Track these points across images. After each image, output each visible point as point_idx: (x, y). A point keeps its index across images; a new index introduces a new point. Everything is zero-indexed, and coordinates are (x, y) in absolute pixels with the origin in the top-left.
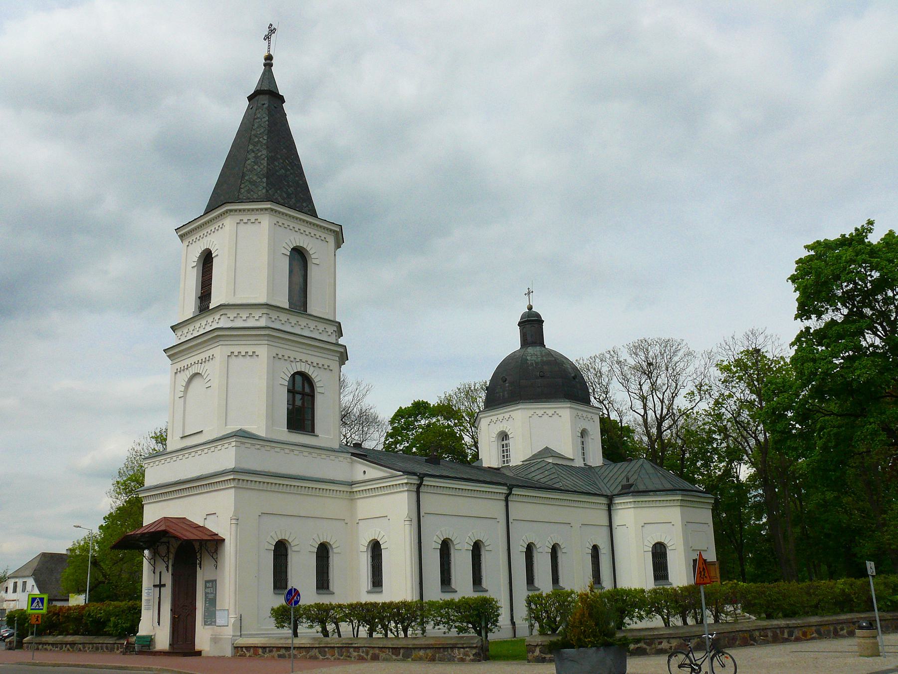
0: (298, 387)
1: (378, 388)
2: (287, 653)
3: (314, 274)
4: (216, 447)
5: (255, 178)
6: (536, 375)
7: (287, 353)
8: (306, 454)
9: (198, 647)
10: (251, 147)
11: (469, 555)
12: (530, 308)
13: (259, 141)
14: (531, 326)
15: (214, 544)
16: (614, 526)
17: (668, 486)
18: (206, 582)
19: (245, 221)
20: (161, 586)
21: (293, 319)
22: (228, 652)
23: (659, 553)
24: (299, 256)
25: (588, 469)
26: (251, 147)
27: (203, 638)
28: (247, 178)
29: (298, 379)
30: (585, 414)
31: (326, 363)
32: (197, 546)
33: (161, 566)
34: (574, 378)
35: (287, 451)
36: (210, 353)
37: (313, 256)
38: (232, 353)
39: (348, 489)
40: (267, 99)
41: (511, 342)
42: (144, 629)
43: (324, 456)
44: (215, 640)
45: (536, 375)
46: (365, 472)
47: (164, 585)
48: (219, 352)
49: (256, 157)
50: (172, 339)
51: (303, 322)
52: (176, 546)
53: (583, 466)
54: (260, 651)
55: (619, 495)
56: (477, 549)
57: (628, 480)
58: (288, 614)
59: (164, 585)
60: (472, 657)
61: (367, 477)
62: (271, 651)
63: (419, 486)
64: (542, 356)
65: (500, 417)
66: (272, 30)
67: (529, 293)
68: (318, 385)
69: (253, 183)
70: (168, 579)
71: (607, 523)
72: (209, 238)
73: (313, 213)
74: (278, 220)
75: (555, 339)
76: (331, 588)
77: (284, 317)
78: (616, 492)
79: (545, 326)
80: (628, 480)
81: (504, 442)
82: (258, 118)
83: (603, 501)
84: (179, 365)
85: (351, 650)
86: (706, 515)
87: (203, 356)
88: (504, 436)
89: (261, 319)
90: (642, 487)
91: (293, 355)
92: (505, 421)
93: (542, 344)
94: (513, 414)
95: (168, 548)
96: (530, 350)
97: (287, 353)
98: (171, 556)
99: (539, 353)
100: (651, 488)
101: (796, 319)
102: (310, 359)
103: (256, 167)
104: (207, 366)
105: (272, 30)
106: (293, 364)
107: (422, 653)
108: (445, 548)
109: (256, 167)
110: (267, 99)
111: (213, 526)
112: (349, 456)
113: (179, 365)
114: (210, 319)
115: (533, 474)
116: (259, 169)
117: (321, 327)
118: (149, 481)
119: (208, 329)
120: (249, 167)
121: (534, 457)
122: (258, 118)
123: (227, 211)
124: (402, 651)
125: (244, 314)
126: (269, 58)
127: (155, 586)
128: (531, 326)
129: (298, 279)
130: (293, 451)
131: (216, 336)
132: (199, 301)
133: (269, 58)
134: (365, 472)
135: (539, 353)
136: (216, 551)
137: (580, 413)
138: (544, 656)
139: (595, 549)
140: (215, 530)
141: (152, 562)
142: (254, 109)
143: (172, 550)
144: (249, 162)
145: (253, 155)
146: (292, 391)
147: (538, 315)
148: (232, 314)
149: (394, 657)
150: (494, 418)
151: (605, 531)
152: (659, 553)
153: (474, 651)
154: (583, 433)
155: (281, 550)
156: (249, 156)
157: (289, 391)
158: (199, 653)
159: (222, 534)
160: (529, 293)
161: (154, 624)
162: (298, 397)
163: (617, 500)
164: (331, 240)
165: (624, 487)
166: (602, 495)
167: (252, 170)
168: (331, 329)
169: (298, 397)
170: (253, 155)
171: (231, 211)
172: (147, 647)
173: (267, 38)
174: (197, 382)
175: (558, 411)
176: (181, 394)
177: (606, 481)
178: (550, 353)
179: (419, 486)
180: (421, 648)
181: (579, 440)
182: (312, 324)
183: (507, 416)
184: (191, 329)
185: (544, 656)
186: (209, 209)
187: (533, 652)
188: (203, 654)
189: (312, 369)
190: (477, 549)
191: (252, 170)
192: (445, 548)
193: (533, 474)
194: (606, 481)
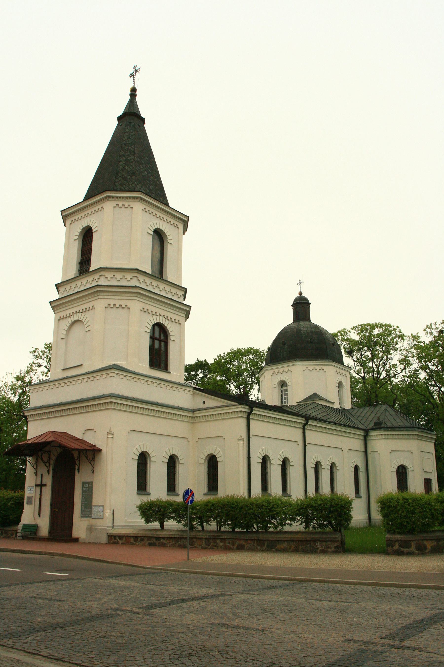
0: (157, 335)
1: (201, 341)
2: (157, 542)
3: (170, 251)
4: (95, 377)
5: (126, 175)
6: (303, 341)
7: (151, 308)
8: (162, 386)
9: (75, 534)
10: (122, 153)
11: (280, 468)
12: (301, 294)
13: (128, 149)
14: (301, 306)
15: (92, 453)
16: (369, 450)
17: (408, 424)
18: (84, 483)
19: (120, 205)
20: (41, 485)
21: (155, 283)
22: (104, 539)
23: (402, 473)
24: (159, 235)
25: (342, 411)
26: (122, 153)
27: (80, 527)
28: (120, 175)
29: (157, 329)
30: (341, 371)
31: (177, 318)
32: (76, 455)
33: (43, 470)
34: (333, 344)
35: (149, 383)
36: (90, 305)
37: (168, 237)
38: (109, 305)
39: (190, 415)
40: (131, 120)
41: (287, 318)
42: (28, 516)
43: (174, 389)
44: (90, 529)
45: (303, 341)
46: (204, 402)
47: (45, 485)
48: (100, 304)
49: (126, 160)
50: (56, 296)
51: (162, 286)
52: (56, 454)
53: (339, 408)
54: (132, 540)
55: (373, 429)
56: (285, 463)
57: (379, 419)
58: (150, 511)
59: (45, 485)
60: (333, 549)
61: (206, 406)
62: (142, 540)
63: (249, 414)
64: (311, 328)
65: (281, 370)
66: (136, 70)
67: (300, 283)
68: (171, 334)
69: (125, 179)
70: (48, 480)
71: (363, 449)
72: (89, 218)
73: (167, 204)
74: (145, 207)
75: (318, 317)
76: (148, 490)
77: (148, 281)
78: (370, 426)
79: (311, 307)
80: (379, 419)
81: (283, 388)
82: (127, 132)
83: (361, 433)
84: (61, 314)
85: (218, 541)
86: (430, 447)
87: (84, 307)
88: (283, 384)
89: (132, 281)
90: (389, 425)
91: (154, 310)
92: (279, 374)
93: (308, 319)
94: (291, 368)
95: (50, 455)
96: (302, 323)
97: (151, 308)
98: (52, 462)
99: (308, 326)
100: (396, 425)
101: (170, 373)
102: (167, 314)
103: (127, 167)
104: (87, 314)
105: (136, 70)
106: (154, 317)
107: (285, 545)
108: (265, 461)
109: (127, 167)
110: (131, 120)
111: (90, 439)
112: (191, 389)
113: (61, 314)
114: (90, 279)
115: (310, 412)
116: (129, 170)
117: (174, 290)
118: (33, 403)
119: (88, 286)
120: (121, 167)
121: (306, 399)
122: (127, 132)
123: (106, 197)
124: (266, 543)
125: (119, 275)
126: (133, 91)
127: (37, 485)
128: (301, 306)
129: (158, 254)
130: (153, 383)
131: (96, 291)
132: (79, 266)
133: (133, 91)
134: (204, 402)
135: (308, 326)
136: (93, 459)
137: (338, 370)
138: (402, 549)
139: (356, 468)
140: (92, 442)
141: (35, 466)
142: (123, 126)
143: (53, 458)
144: (121, 163)
145: (124, 158)
146: (152, 338)
147: (306, 299)
148: (109, 275)
149: (259, 548)
150: (276, 371)
151: (362, 455)
152: (402, 473)
153: (336, 545)
154: (340, 385)
155: (143, 459)
156: (121, 159)
157: (151, 337)
158: (76, 540)
159: (99, 446)
160: (300, 283)
161: (35, 514)
162: (157, 342)
163: (372, 433)
164: (181, 226)
165: (376, 424)
166: (359, 429)
167: (124, 169)
168: (181, 293)
169: (157, 342)
170: (124, 158)
171: (109, 197)
172: (31, 533)
173: (133, 75)
174: (77, 328)
175: (324, 367)
176: (63, 336)
177: (360, 419)
178: (316, 326)
179: (249, 414)
180: (284, 541)
181: (337, 389)
182: (168, 288)
183: (286, 369)
184: (73, 287)
185: (402, 549)
186: (88, 197)
187: (393, 546)
188: (80, 541)
189: (167, 321)
190: (285, 463)
191: (124, 169)
192: (265, 461)
193: (310, 412)
194: (360, 419)
